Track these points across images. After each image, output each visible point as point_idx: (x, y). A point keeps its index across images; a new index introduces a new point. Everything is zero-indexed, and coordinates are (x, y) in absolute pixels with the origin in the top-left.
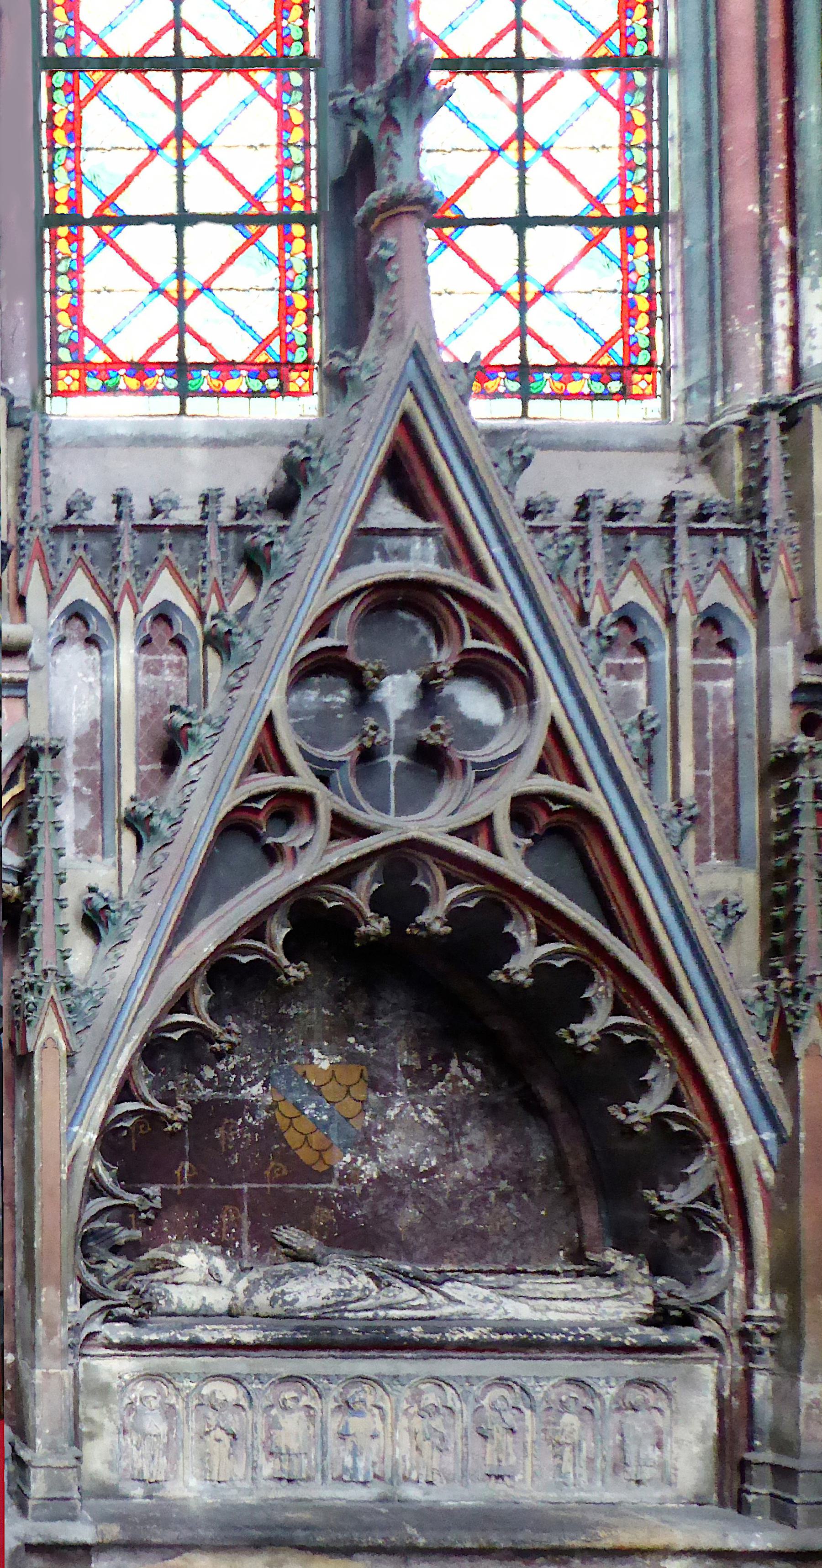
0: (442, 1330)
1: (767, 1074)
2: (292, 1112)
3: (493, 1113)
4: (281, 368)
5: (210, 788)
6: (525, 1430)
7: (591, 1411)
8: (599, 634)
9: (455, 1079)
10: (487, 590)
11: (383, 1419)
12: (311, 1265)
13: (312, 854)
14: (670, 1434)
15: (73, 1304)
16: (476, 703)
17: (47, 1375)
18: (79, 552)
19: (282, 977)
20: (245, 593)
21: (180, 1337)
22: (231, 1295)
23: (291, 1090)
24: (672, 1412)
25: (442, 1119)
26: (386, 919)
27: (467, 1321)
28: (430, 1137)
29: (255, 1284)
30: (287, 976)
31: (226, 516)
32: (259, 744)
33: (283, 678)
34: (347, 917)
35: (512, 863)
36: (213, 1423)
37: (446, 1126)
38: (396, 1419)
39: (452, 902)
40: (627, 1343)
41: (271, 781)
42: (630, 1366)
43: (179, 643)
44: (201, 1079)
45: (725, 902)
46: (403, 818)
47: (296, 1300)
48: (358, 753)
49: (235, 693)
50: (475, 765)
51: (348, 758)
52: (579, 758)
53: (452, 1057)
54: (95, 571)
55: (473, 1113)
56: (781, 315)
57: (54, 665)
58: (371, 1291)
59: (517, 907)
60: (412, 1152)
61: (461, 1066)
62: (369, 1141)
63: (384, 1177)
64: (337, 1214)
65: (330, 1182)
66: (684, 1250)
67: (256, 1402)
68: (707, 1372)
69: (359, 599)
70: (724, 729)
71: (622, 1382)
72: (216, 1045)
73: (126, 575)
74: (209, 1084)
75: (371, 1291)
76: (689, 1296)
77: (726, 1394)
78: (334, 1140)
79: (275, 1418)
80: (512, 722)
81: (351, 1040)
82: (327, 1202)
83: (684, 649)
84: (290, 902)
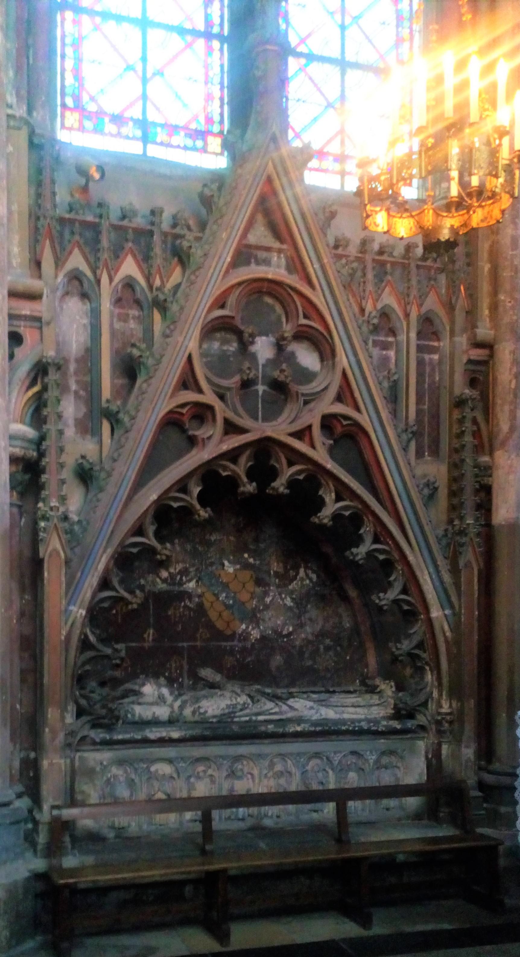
0: (284, 726)
1: (447, 578)
2: (211, 598)
3: (322, 599)
4: (204, 134)
5: (158, 398)
7: (363, 770)
9: (302, 579)
10: (311, 290)
11: (253, 781)
13: (213, 444)
15: (69, 719)
16: (307, 358)
17: (51, 764)
18: (77, 237)
19: (197, 516)
20: (176, 276)
23: (212, 585)
25: (296, 603)
26: (254, 484)
27: (299, 720)
29: (184, 703)
30: (199, 515)
31: (166, 226)
32: (183, 373)
33: (197, 333)
34: (233, 482)
35: (321, 455)
37: (298, 607)
38: (260, 780)
39: (290, 476)
40: (380, 730)
41: (191, 396)
42: (382, 743)
43: (138, 303)
44: (160, 578)
45: (428, 481)
46: (266, 424)
47: (206, 712)
48: (240, 383)
49: (168, 340)
50: (303, 395)
51: (233, 386)
52: (357, 394)
53: (300, 567)
55: (312, 599)
58: (248, 704)
60: (279, 622)
61: (305, 571)
62: (255, 616)
63: (264, 638)
64: (237, 660)
65: (233, 641)
68: (421, 745)
70: (434, 382)
71: (379, 752)
73: (105, 256)
74: (164, 581)
75: (248, 704)
76: (411, 702)
79: (193, 784)
80: (324, 371)
81: (246, 555)
82: (232, 652)
83: (413, 335)
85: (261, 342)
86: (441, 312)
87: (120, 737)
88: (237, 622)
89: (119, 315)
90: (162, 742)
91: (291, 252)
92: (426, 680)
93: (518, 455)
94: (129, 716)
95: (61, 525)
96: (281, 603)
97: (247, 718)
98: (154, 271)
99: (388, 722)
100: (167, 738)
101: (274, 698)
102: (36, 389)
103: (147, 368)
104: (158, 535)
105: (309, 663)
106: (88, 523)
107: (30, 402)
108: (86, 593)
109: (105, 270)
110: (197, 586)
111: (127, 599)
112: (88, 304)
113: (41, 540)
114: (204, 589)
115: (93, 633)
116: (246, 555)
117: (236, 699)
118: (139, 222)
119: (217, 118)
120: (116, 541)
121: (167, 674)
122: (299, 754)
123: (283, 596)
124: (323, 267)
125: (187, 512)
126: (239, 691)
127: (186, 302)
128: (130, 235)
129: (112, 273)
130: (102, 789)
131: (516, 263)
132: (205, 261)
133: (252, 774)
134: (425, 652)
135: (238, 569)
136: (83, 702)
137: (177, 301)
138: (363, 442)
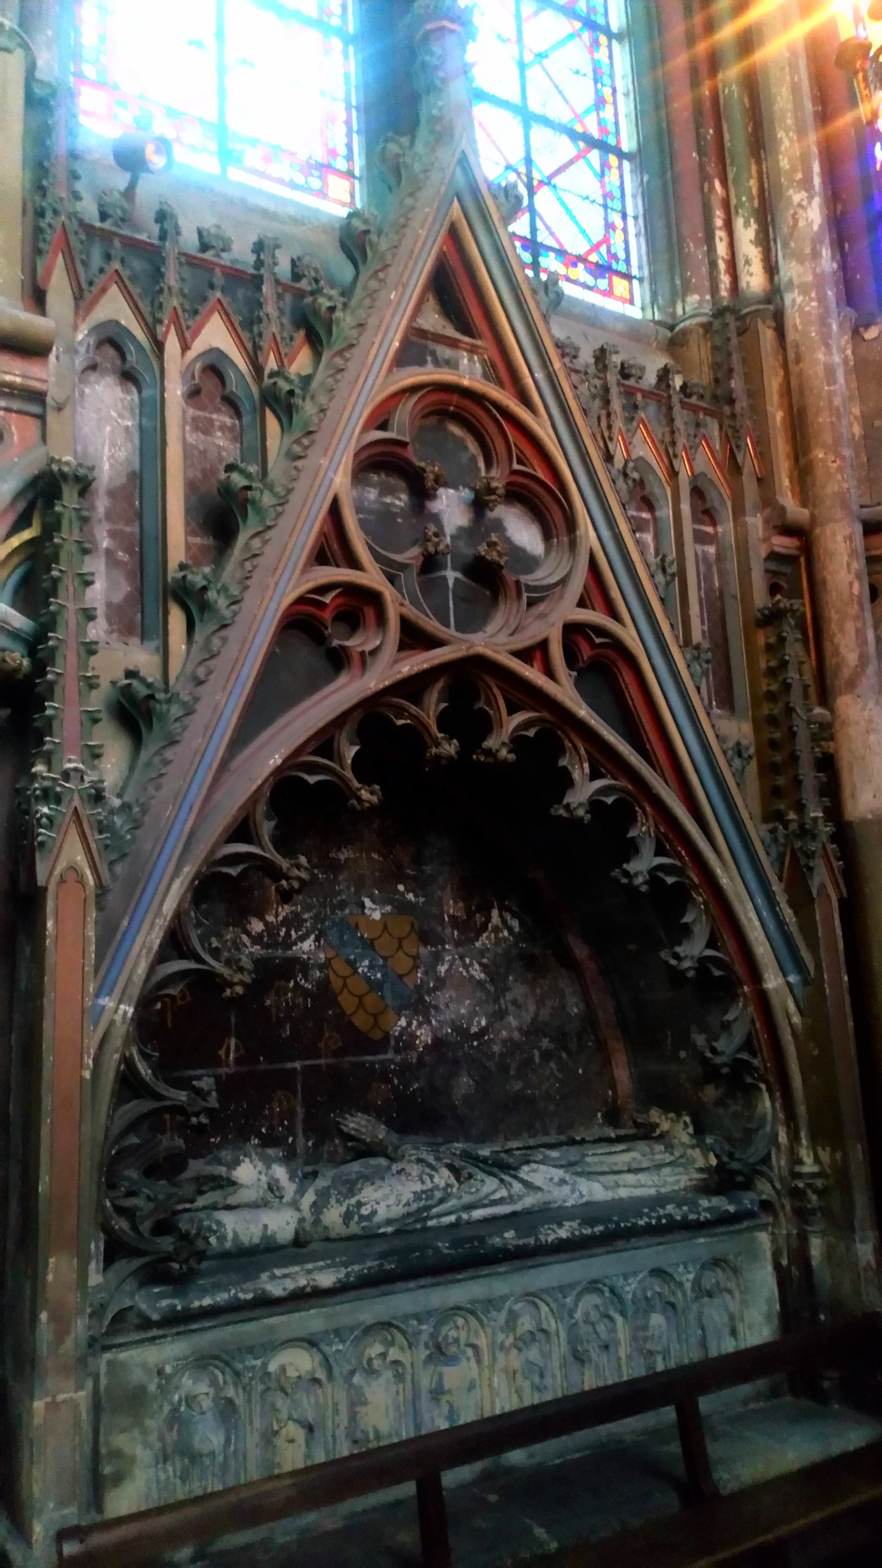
0: (533, 1230)
2: (346, 971)
3: (533, 966)
4: (326, 168)
5: (277, 575)
6: (617, 1343)
7: (673, 1305)
8: (625, 475)
11: (479, 1361)
12: (383, 1161)
13: (384, 666)
14: (742, 1319)
16: (523, 533)
17: (53, 1406)
19: (354, 802)
20: (301, 362)
21: (241, 1296)
22: (297, 1215)
23: (343, 944)
24: (741, 1292)
27: (550, 1214)
28: (479, 994)
29: (323, 1197)
30: (360, 800)
31: (284, 269)
32: (322, 534)
34: (416, 735)
35: (565, 690)
36: (284, 1415)
38: (494, 1359)
39: (515, 730)
40: (702, 1218)
43: (232, 404)
44: (248, 934)
47: (374, 1213)
49: (299, 463)
50: (529, 588)
52: (615, 593)
54: (135, 291)
56: (722, 249)
57: (82, 394)
59: (571, 741)
60: (463, 1011)
61: (501, 916)
62: (421, 1000)
63: (438, 1043)
65: (386, 1052)
66: (719, 1103)
67: (336, 1371)
68: (764, 1238)
69: (419, 394)
72: (284, 883)
74: (257, 939)
77: (785, 1262)
78: (389, 1001)
79: (359, 1390)
80: (553, 554)
81: (401, 888)
84: (358, 715)
85: (448, 497)
86: (717, 476)
87: (207, 1301)
88: (391, 1014)
89: (194, 419)
90: (300, 1299)
91: (492, 352)
92: (759, 1109)
93: (877, 703)
94: (213, 1240)
95: (86, 812)
96: (465, 974)
97: (452, 1218)
98: (265, 343)
99: (710, 1202)
100: (309, 1290)
101: (501, 1167)
102: (27, 535)
103: (259, 511)
104: (283, 844)
105: (518, 1086)
106: (144, 811)
107: (15, 560)
108: (136, 965)
109: (172, 328)
110: (318, 947)
111: (221, 976)
112: (134, 390)
113: (42, 844)
114: (331, 953)
115: (145, 1056)
116: (401, 888)
117: (431, 1177)
118: (241, 253)
119: (342, 151)
120: (201, 851)
121: (263, 1130)
122: (564, 1289)
123: (468, 961)
124: (551, 378)
125: (334, 793)
126: (431, 1159)
127: (330, 400)
128: (219, 279)
129: (188, 335)
130: (161, 1438)
131: (836, 403)
132: (360, 335)
133: (474, 1347)
134: (755, 1056)
135: (388, 914)
136: (121, 1224)
137: (312, 398)
138: (627, 678)
